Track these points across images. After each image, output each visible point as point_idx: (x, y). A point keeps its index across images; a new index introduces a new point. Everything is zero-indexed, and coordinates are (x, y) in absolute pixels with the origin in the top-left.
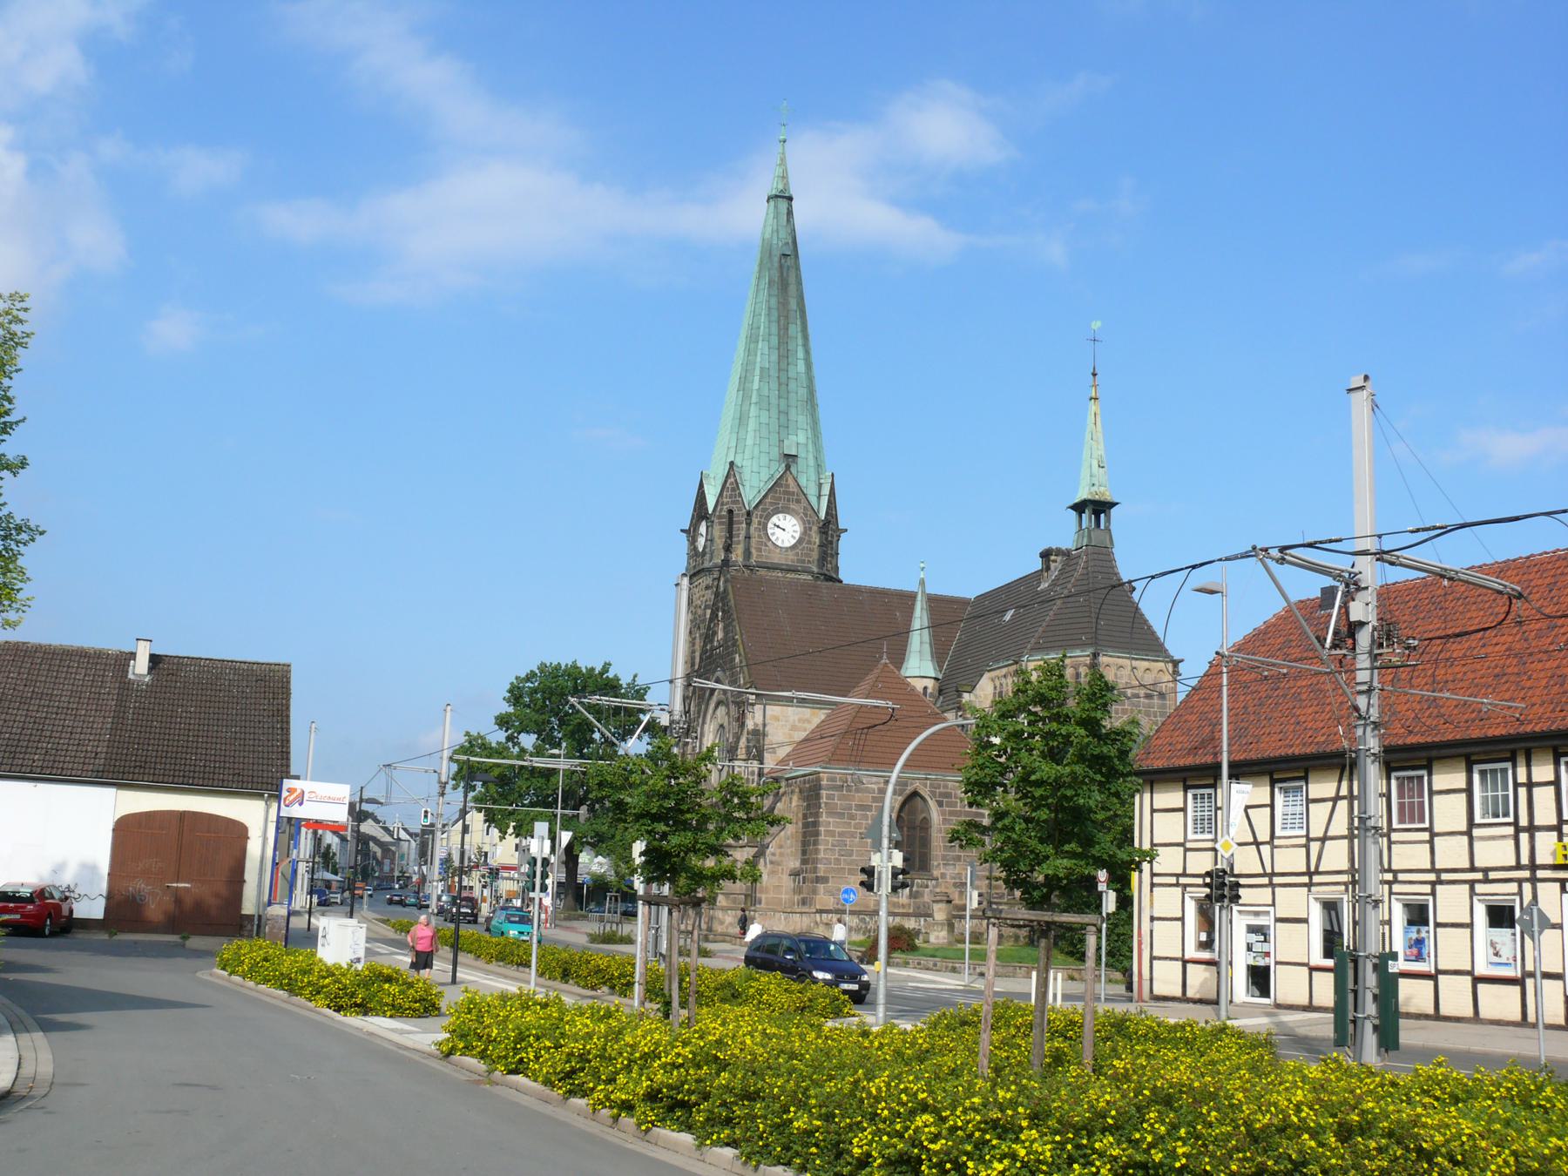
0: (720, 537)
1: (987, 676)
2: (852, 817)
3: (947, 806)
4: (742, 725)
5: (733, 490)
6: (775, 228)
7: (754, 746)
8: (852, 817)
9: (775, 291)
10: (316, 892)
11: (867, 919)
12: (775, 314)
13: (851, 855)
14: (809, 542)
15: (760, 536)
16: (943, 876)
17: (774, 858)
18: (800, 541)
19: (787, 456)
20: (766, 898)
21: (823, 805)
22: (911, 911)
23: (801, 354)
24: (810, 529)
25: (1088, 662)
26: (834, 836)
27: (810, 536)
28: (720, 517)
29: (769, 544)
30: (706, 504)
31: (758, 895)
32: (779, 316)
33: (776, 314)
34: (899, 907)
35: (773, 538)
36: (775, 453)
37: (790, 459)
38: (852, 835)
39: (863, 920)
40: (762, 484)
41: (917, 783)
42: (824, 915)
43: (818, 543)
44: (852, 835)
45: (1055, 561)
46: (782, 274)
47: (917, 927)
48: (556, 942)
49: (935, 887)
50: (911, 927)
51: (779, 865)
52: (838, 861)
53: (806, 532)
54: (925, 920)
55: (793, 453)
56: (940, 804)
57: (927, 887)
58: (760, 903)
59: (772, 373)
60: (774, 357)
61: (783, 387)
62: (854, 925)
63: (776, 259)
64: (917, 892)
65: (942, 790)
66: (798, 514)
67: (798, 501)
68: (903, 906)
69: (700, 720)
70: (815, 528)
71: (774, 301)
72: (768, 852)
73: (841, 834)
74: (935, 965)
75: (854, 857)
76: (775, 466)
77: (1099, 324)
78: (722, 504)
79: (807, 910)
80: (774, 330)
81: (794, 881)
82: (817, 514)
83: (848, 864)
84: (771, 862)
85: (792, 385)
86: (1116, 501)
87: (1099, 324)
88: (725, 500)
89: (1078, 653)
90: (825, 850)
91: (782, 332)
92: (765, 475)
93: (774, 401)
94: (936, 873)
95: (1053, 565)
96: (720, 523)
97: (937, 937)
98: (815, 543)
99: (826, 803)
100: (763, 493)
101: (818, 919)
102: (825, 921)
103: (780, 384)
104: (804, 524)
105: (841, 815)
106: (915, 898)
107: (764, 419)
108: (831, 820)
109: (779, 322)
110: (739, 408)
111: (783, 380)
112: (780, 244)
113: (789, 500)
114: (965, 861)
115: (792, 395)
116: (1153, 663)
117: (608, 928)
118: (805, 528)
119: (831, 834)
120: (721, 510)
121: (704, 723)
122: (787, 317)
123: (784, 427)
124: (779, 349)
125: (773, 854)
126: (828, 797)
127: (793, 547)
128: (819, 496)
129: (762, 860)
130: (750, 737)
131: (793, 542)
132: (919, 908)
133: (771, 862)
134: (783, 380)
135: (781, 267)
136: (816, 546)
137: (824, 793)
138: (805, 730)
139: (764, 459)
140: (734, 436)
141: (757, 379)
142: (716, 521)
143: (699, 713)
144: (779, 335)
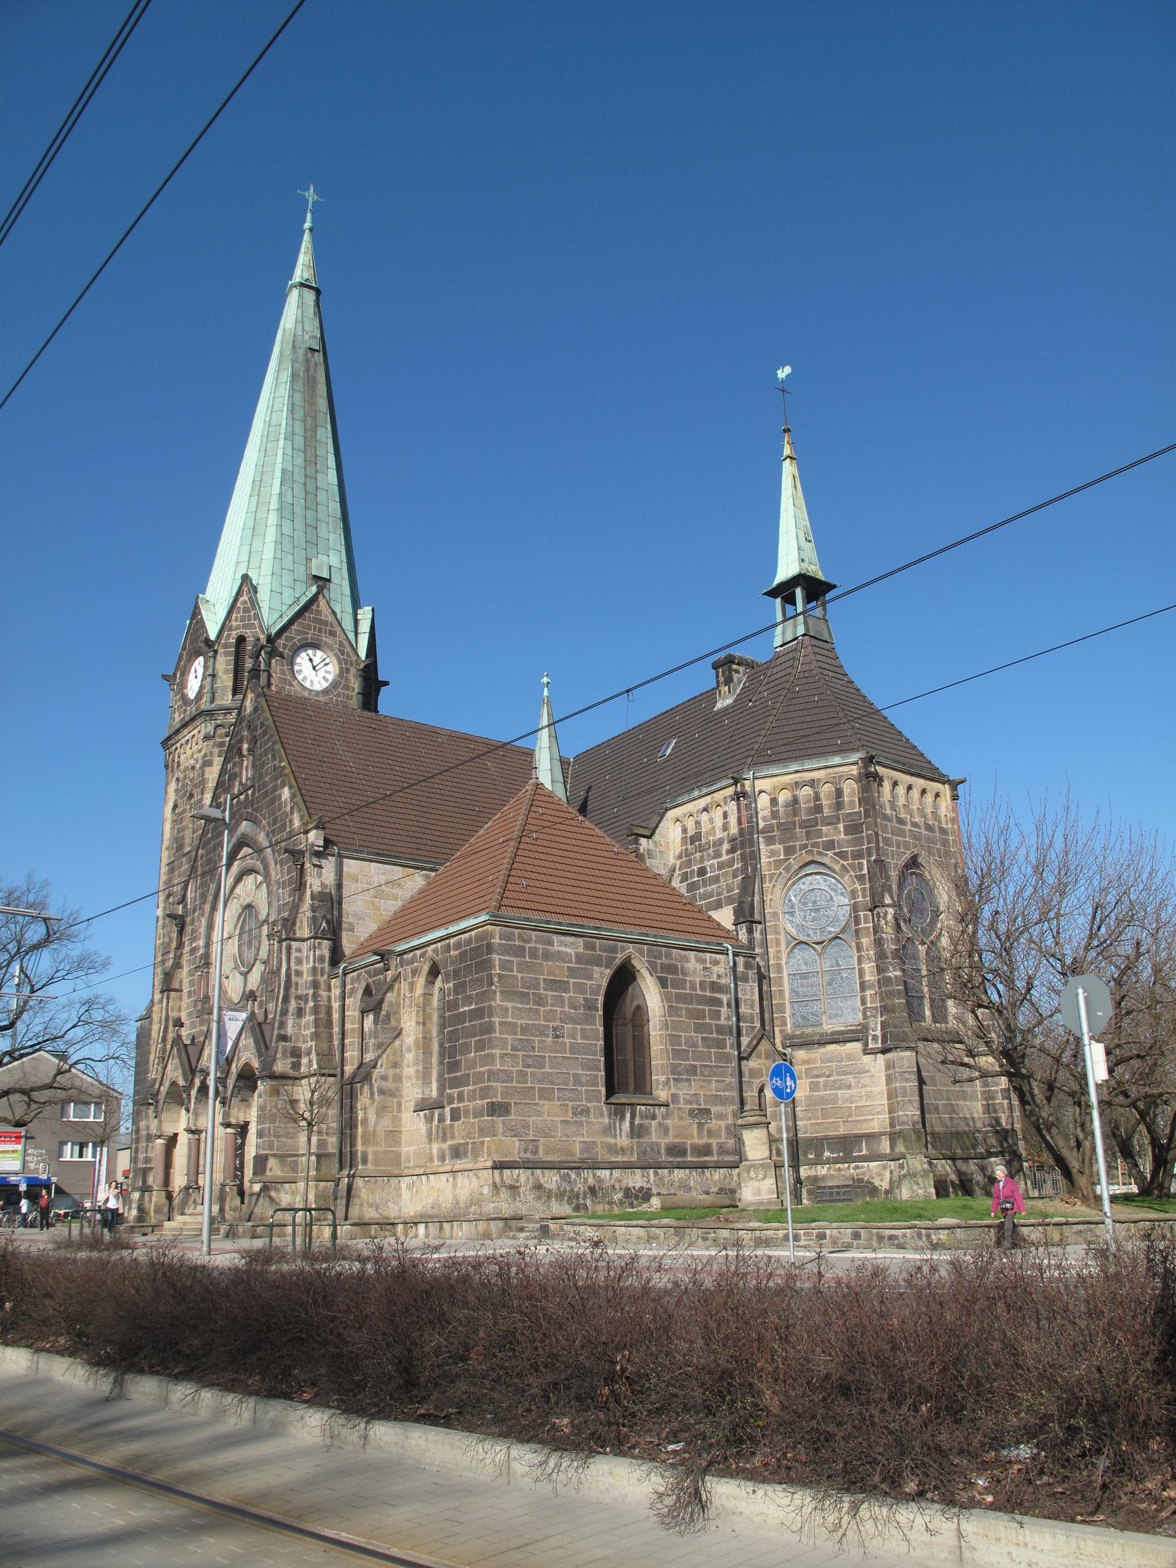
0: (226, 672)
1: (671, 814)
2: (540, 1001)
3: (673, 987)
4: (301, 886)
5: (246, 610)
6: (300, 318)
7: (324, 917)
8: (540, 1001)
9: (299, 386)
10: (328, 1402)
11: (573, 1176)
12: (299, 414)
13: (542, 1066)
14: (346, 687)
15: (282, 672)
16: (675, 1097)
17: (384, 1084)
18: (335, 685)
19: (317, 578)
20: (375, 1153)
21: (496, 979)
22: (634, 1158)
23: (332, 462)
24: (348, 671)
25: (855, 772)
26: (515, 1033)
27: (347, 679)
28: (226, 646)
29: (294, 683)
30: (203, 626)
31: (360, 1148)
32: (305, 416)
33: (302, 413)
34: (616, 1152)
35: (300, 677)
36: (301, 571)
37: (322, 582)
38: (542, 1032)
39: (565, 1178)
40: (284, 608)
41: (631, 949)
42: (507, 1172)
43: (357, 690)
44: (542, 1032)
45: (737, 672)
46: (308, 370)
47: (645, 1185)
48: (1083, 1055)
49: (664, 1117)
50: (638, 1185)
51: (393, 1095)
52: (522, 1074)
53: (343, 672)
54: (656, 1174)
55: (325, 575)
56: (663, 983)
57: (654, 1117)
58: (365, 1162)
59: (296, 477)
60: (299, 460)
61: (311, 497)
62: (553, 1186)
63: (301, 352)
64: (641, 1126)
65: (664, 961)
66: (333, 650)
67: (332, 634)
68: (623, 1150)
69: (207, 907)
70: (353, 671)
71: (298, 397)
72: (376, 1073)
73: (525, 1029)
74: (856, 1236)
75: (547, 1070)
76: (300, 588)
77: (788, 370)
78: (231, 629)
79: (470, 1166)
80: (299, 428)
81: (429, 1120)
82: (355, 651)
83: (540, 1081)
84: (382, 1092)
85: (322, 496)
86: (832, 582)
87: (788, 370)
88: (234, 624)
89: (837, 760)
90: (503, 1056)
91: (309, 434)
92: (288, 598)
93: (299, 510)
94: (662, 1095)
95: (735, 676)
96: (226, 654)
97: (758, 1192)
98: (353, 689)
99: (499, 975)
100: (286, 619)
101: (498, 1180)
102: (508, 1182)
103: (307, 492)
104: (340, 663)
105: (524, 997)
106: (639, 1136)
107: (287, 529)
108: (509, 1005)
109: (305, 421)
110: (252, 515)
111: (310, 488)
112: (307, 337)
113: (320, 631)
114: (702, 1074)
115: (321, 509)
116: (929, 782)
117: (87, 1231)
118: (341, 668)
119: (509, 1027)
120: (228, 637)
121: (214, 908)
122: (315, 418)
123: (313, 543)
124: (305, 452)
125: (384, 1078)
126: (505, 966)
127: (325, 692)
128: (356, 634)
129: (366, 1088)
130: (317, 903)
131: (325, 685)
132: (644, 1153)
133: (382, 1092)
134: (310, 488)
135: (307, 361)
136: (354, 694)
137: (496, 957)
138: (396, 899)
139: (287, 579)
140: (246, 549)
141: (277, 482)
142: (221, 650)
143: (204, 897)
144: (305, 437)
